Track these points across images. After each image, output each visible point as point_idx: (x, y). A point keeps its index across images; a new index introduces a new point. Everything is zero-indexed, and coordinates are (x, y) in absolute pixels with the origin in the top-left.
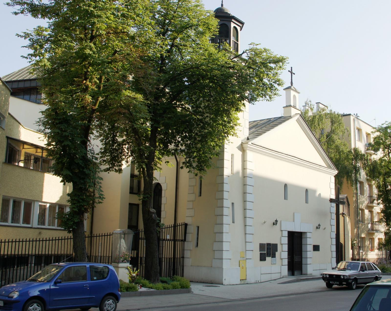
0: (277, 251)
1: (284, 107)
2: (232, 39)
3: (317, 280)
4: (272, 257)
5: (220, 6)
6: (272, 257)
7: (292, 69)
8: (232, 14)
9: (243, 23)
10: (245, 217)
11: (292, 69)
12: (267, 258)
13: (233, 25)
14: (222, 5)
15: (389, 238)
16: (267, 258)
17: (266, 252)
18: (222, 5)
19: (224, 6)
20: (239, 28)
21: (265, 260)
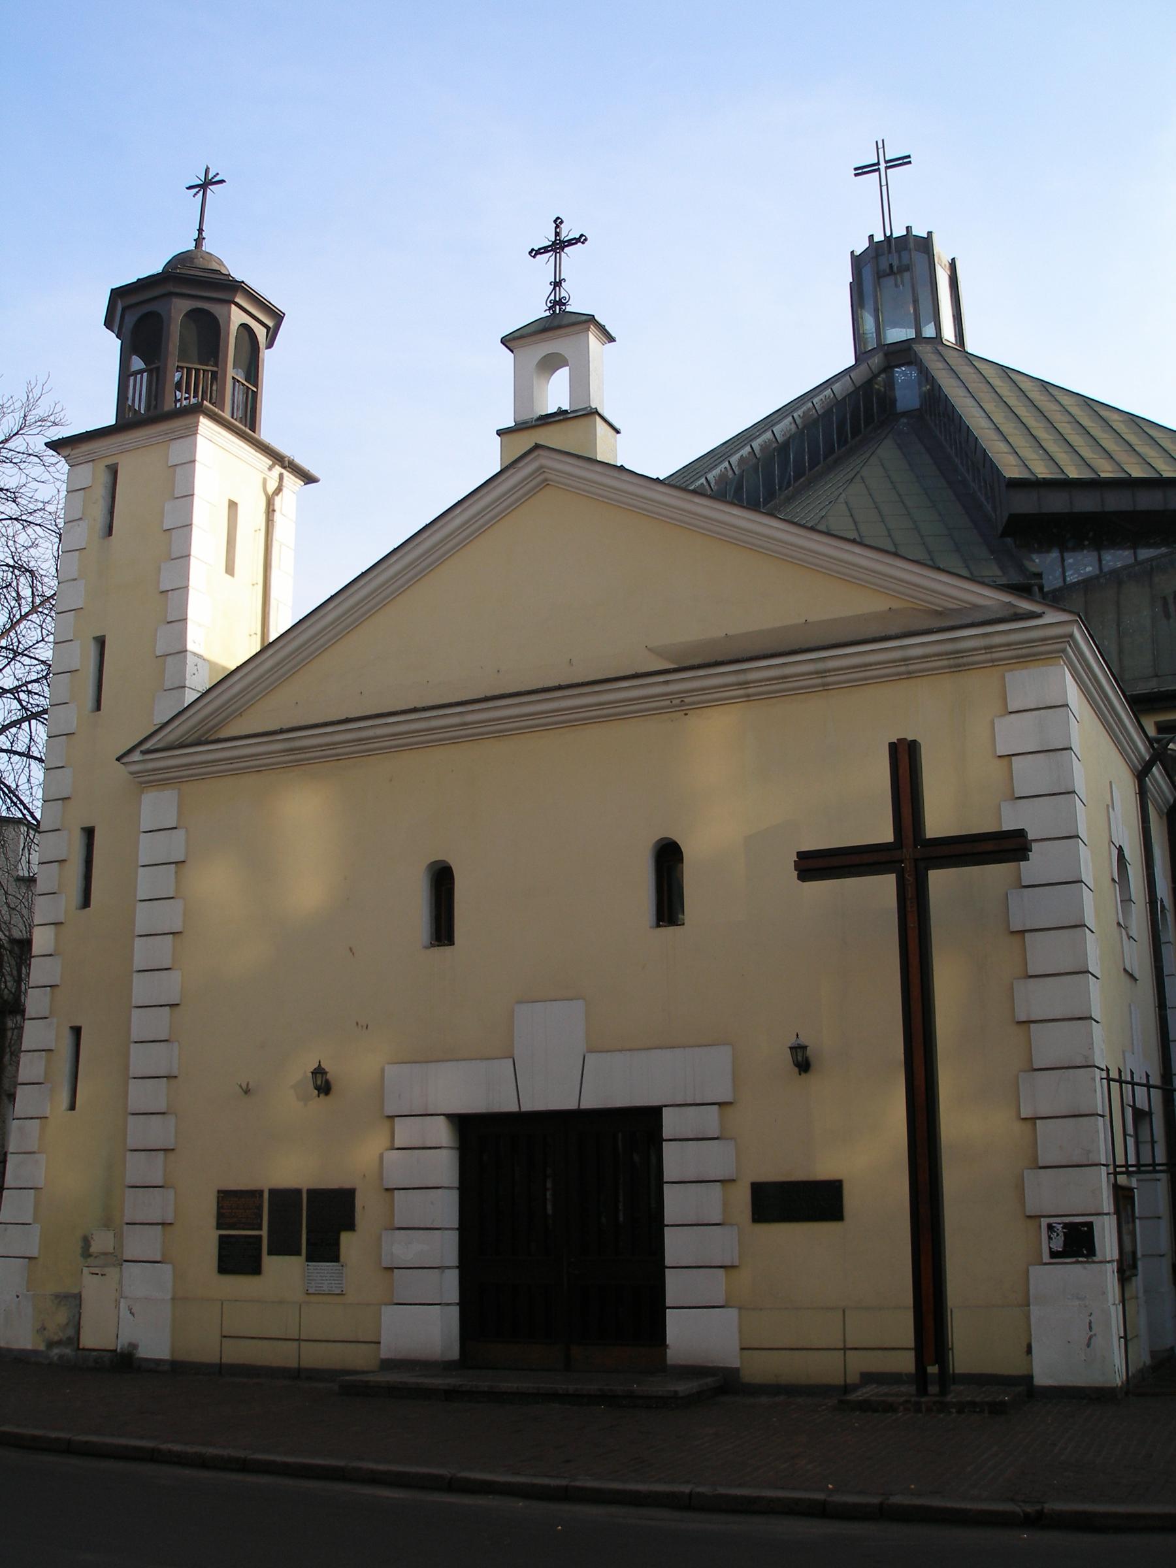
0: (351, 1226)
1: (500, 433)
2: (232, 372)
3: (234, 547)
4: (309, 1259)
5: (191, 246)
6: (309, 1259)
7: (576, 241)
8: (238, 275)
9: (278, 317)
10: (890, 536)
11: (576, 241)
12: (270, 1263)
13: (237, 317)
14: (199, 241)
15: (82, 656)
16: (270, 1263)
17: (264, 1233)
18: (199, 241)
19: (207, 247)
20: (261, 332)
21: (254, 1268)
